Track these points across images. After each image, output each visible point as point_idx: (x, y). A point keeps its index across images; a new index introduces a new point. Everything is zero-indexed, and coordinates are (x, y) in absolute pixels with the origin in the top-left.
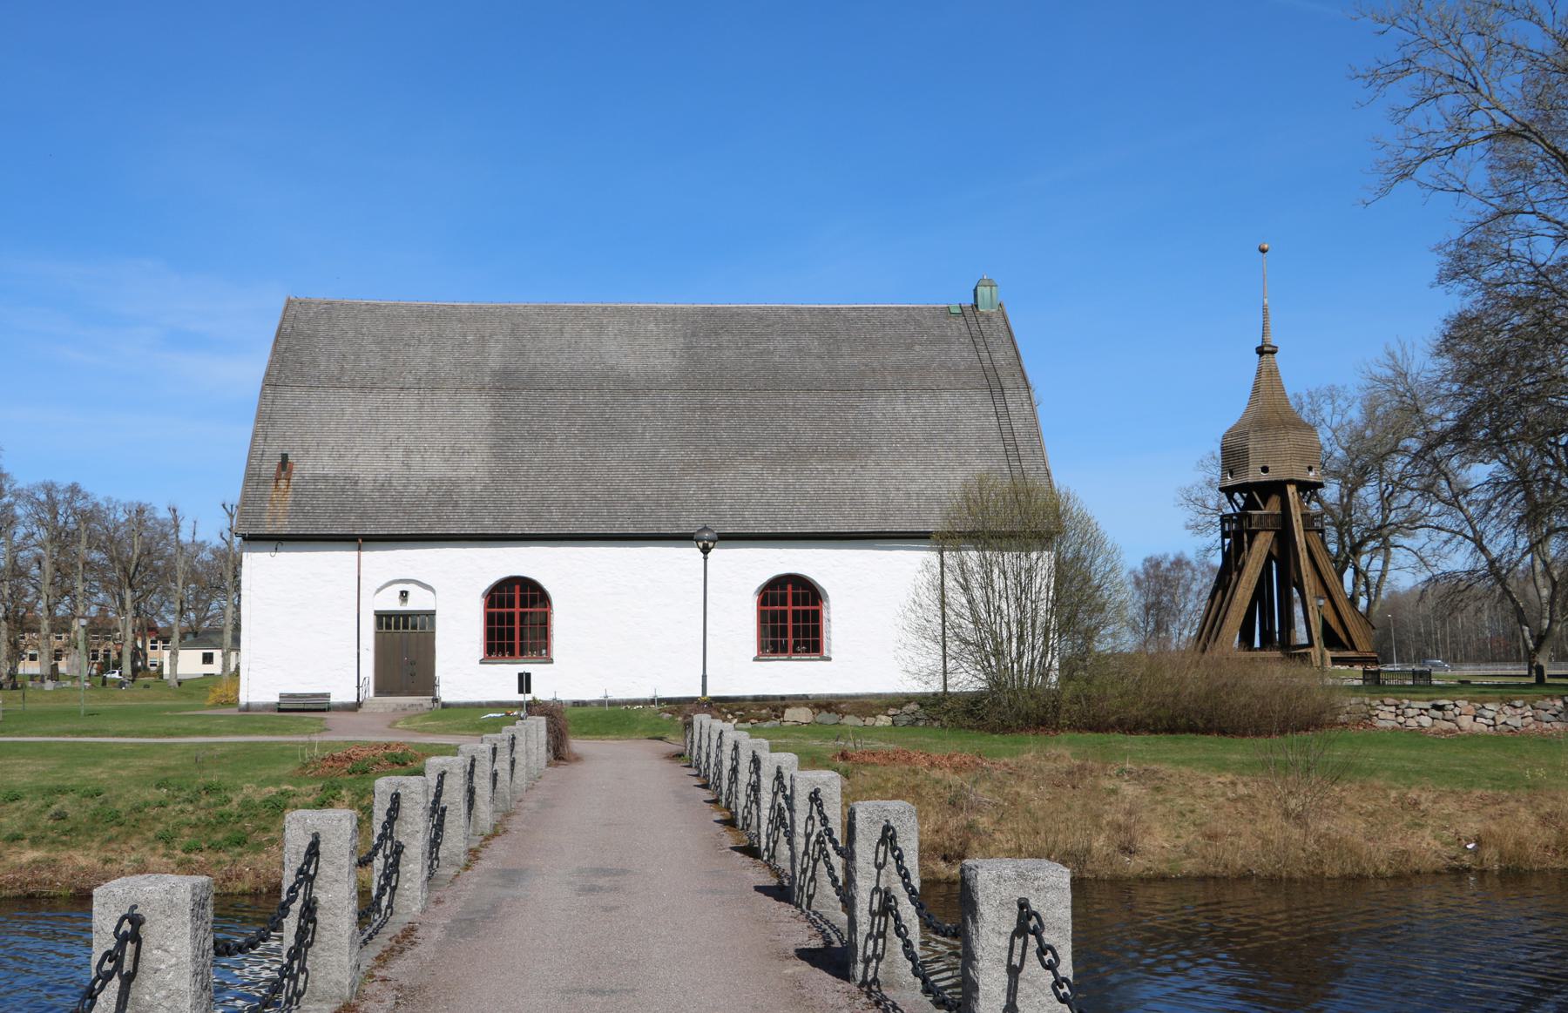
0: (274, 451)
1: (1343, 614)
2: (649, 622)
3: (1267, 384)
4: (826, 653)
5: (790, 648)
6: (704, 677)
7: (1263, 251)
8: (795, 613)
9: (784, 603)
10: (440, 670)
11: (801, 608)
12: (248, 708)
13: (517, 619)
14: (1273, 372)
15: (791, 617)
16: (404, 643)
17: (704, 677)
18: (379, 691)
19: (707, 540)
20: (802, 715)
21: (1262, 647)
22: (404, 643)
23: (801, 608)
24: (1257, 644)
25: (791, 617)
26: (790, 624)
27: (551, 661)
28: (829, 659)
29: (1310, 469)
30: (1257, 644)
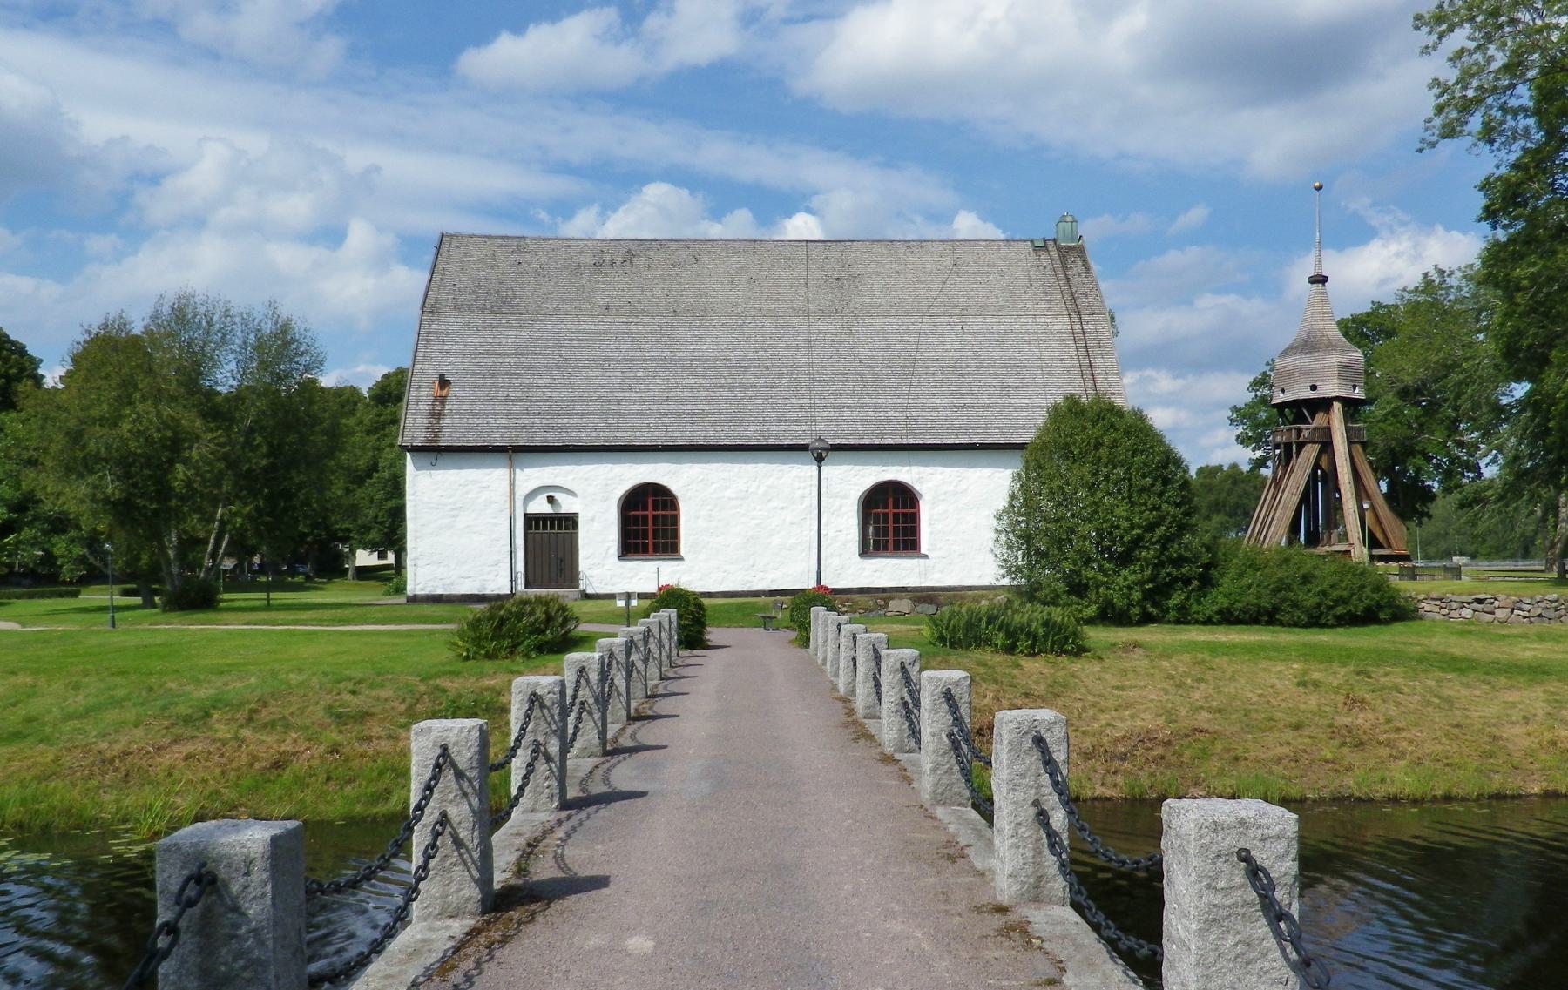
1: (1381, 514)
4: (923, 550)
5: (891, 546)
6: (819, 573)
7: (1319, 188)
9: (886, 507)
10: (583, 565)
12: (414, 599)
15: (891, 520)
16: (549, 540)
17: (819, 573)
18: (527, 585)
19: (820, 453)
22: (549, 540)
25: (891, 520)
26: (891, 525)
27: (865, 552)
28: (926, 556)
29: (1355, 387)
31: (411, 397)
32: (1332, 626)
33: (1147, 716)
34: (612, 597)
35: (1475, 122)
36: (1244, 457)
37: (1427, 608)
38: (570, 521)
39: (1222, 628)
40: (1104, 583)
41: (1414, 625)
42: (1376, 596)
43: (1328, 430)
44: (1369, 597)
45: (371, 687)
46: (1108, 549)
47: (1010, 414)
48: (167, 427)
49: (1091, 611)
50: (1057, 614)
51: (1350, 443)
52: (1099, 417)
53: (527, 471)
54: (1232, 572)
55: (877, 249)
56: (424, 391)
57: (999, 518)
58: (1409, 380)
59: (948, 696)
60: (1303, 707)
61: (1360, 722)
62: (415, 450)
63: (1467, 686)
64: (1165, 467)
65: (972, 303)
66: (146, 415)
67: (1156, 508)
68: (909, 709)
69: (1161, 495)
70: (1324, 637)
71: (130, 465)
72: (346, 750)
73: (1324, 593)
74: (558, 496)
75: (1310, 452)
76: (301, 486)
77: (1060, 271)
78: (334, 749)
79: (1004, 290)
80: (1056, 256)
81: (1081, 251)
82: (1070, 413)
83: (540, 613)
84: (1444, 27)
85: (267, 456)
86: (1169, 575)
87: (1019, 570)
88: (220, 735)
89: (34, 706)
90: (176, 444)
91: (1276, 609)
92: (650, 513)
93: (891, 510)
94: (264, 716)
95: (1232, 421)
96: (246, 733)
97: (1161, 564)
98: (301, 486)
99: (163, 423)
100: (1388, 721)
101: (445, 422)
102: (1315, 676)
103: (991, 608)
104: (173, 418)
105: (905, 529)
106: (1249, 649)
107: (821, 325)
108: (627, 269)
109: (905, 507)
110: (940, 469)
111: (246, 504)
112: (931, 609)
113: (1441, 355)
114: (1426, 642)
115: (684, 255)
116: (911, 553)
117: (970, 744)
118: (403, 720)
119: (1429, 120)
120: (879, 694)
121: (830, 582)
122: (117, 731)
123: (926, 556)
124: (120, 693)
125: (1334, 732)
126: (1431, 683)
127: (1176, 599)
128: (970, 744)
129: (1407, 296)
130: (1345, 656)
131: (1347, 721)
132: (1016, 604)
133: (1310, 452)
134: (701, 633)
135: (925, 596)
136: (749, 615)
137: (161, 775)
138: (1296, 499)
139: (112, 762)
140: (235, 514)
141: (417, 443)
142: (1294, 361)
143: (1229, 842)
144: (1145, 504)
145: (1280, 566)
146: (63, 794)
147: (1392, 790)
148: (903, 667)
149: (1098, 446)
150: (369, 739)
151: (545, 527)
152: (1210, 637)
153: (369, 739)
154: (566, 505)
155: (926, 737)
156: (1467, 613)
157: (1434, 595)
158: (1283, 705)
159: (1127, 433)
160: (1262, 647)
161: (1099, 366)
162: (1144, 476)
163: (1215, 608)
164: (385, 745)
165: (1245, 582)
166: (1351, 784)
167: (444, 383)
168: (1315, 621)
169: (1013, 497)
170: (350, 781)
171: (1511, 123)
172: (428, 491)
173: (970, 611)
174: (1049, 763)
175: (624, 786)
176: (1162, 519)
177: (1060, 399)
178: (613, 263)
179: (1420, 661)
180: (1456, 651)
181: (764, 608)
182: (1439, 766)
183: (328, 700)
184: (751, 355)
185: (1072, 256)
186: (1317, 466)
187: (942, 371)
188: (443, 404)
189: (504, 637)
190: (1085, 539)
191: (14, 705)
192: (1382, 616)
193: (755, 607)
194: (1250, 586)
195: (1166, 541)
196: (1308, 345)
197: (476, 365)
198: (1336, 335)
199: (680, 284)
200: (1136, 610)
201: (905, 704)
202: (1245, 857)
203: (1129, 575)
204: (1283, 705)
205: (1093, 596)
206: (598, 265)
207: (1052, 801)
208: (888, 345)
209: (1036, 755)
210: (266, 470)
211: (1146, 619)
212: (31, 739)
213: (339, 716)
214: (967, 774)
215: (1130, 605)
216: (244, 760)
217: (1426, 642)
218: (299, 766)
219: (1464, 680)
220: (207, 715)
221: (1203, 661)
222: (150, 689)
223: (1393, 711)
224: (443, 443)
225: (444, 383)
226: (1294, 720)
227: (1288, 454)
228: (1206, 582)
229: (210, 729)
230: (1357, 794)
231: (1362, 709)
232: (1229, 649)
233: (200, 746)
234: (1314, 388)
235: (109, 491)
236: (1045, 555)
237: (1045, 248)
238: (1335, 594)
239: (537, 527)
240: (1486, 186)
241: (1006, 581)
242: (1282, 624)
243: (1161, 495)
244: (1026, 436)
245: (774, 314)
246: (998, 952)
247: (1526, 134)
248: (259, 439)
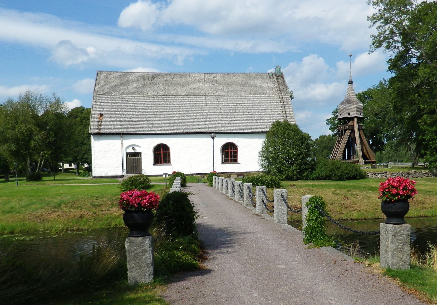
1: (368, 149)
4: (239, 162)
5: (230, 160)
6: (213, 168)
7: (351, 56)
12: (95, 177)
15: (230, 153)
16: (133, 160)
17: (213, 168)
19: (213, 135)
21: (348, 159)
22: (133, 160)
24: (346, 158)
25: (230, 153)
26: (230, 155)
27: (222, 163)
29: (360, 114)
30: (346, 158)
31: (92, 119)
32: (345, 180)
33: (296, 202)
34: (161, 176)
35: (385, 44)
36: (330, 133)
37: (370, 175)
38: (139, 155)
39: (317, 181)
40: (287, 170)
41: (366, 180)
42: (356, 172)
43: (353, 126)
44: (354, 173)
45: (101, 198)
46: (288, 161)
47: (263, 123)
48: (29, 131)
49: (284, 177)
50: (274, 177)
51: (359, 130)
52: (285, 126)
53: (127, 141)
54: (320, 166)
55: (224, 75)
56: (96, 118)
57: (259, 153)
58: (376, 112)
59: (248, 187)
60: (333, 199)
61: (347, 202)
62: (94, 135)
63: (374, 194)
64: (302, 139)
65: (252, 92)
66: (22, 127)
67: (300, 150)
68: (241, 194)
69: (301, 147)
70: (342, 183)
71: (18, 141)
72: (98, 213)
73: (343, 172)
74: (135, 147)
75: (348, 133)
76: (64, 145)
77: (276, 82)
78: (95, 213)
79: (261, 88)
80: (275, 78)
81: (282, 76)
82: (277, 125)
83: (142, 179)
84: (375, 21)
85: (54, 137)
86: (303, 167)
87: (265, 167)
88: (64, 210)
89: (12, 204)
90: (30, 135)
91: (330, 176)
93: (230, 151)
94: (75, 205)
95: (327, 123)
96: (71, 210)
97: (301, 165)
98: (64, 145)
99: (28, 129)
100: (353, 202)
101: (103, 126)
102: (338, 192)
103: (257, 176)
104: (30, 128)
105: (234, 156)
106: (322, 186)
107: (209, 98)
108: (153, 82)
109: (234, 150)
110: (243, 139)
111: (49, 151)
112: (242, 177)
113: (385, 104)
114: (367, 184)
115: (169, 77)
116: (235, 162)
117: (252, 195)
118: (111, 206)
119: (371, 46)
122: (37, 210)
124: (34, 201)
125: (340, 205)
126: (365, 193)
127: (305, 174)
128: (252, 195)
129: (375, 87)
130: (345, 187)
131: (344, 202)
132: (264, 175)
133: (348, 133)
134: (185, 183)
135: (240, 174)
136: (194, 179)
137: (52, 220)
138: (344, 146)
139: (38, 217)
140: (46, 154)
141: (94, 133)
142: (344, 106)
143: (280, 193)
144: (297, 149)
145: (332, 165)
146: (30, 225)
147: (352, 217)
149: (284, 134)
150: (103, 210)
151: (132, 156)
152: (313, 183)
153: (103, 210)
154: (138, 150)
156: (379, 176)
157: (371, 172)
158: (329, 199)
159: (292, 130)
160: (326, 185)
161: (287, 109)
162: (297, 142)
163: (315, 176)
164: (107, 212)
165: (323, 169)
166: (343, 217)
167: (101, 115)
168: (340, 179)
169: (263, 147)
170: (100, 220)
171: (394, 44)
172: (98, 147)
173: (252, 177)
174: (263, 192)
176: (301, 153)
177: (275, 122)
178: (148, 80)
179: (364, 188)
180: (374, 186)
181: (198, 178)
182: (364, 212)
183: (91, 201)
184: (189, 107)
185: (280, 78)
186: (350, 136)
187: (243, 111)
188: (101, 121)
189: (133, 185)
190: (282, 158)
191: (5, 204)
192: (358, 177)
193: (196, 178)
194: (324, 170)
195: (302, 159)
196: (348, 102)
197: (111, 110)
198: (355, 99)
199: (168, 86)
200: (295, 177)
201: (240, 192)
202: (281, 194)
203: (294, 167)
204: (329, 199)
205: (284, 173)
206: (144, 80)
207: (264, 198)
208: (228, 104)
209: (262, 192)
210: (54, 141)
211: (298, 179)
212: (14, 212)
213: (94, 205)
214: (252, 199)
215: (294, 175)
216: (72, 216)
217: (367, 184)
218: (86, 217)
219: (373, 192)
220: (60, 206)
221: (310, 189)
222: (42, 200)
223: (355, 200)
224: (102, 133)
225: (101, 115)
226: (331, 202)
227: (342, 133)
228: (313, 169)
229: (62, 209)
230: (344, 218)
231: (348, 199)
232: (317, 186)
233: (60, 213)
234: (349, 114)
235: (12, 148)
236: (271, 162)
237: (272, 75)
238: (345, 172)
239: (130, 156)
240: (390, 61)
241: (261, 170)
242: (332, 180)
243: (301, 147)
244: (267, 130)
245: (196, 95)
246: (258, 217)
247: (398, 48)
248: (51, 133)
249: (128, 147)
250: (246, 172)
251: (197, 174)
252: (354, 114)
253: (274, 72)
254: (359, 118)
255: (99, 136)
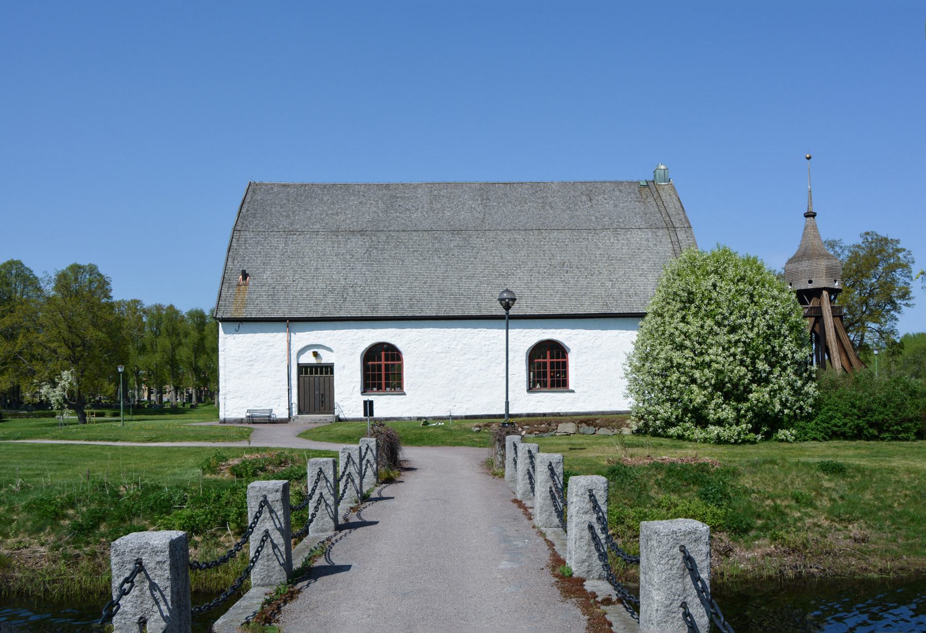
0: (236, 267)
2: (460, 372)
3: (810, 233)
4: (571, 387)
5: (549, 383)
6: (507, 403)
7: (809, 158)
8: (552, 363)
10: (337, 399)
11: (561, 360)
12: (225, 421)
13: (382, 368)
14: (815, 227)
15: (548, 367)
16: (315, 382)
17: (507, 403)
20: (570, 427)
22: (315, 382)
23: (561, 360)
25: (548, 367)
27: (530, 389)
28: (573, 391)
62: (224, 320)
74: (320, 351)
92: (383, 363)
110: (583, 331)
116: (561, 389)
120: (533, 488)
121: (512, 411)
123: (573, 391)
148: (550, 464)
151: (316, 373)
154: (326, 358)
155: (537, 493)
175: (368, 519)
249: (302, 352)
250: (603, 413)
251: (467, 417)
252: (821, 282)
253: (652, 178)
254: (833, 292)
255: (236, 325)
